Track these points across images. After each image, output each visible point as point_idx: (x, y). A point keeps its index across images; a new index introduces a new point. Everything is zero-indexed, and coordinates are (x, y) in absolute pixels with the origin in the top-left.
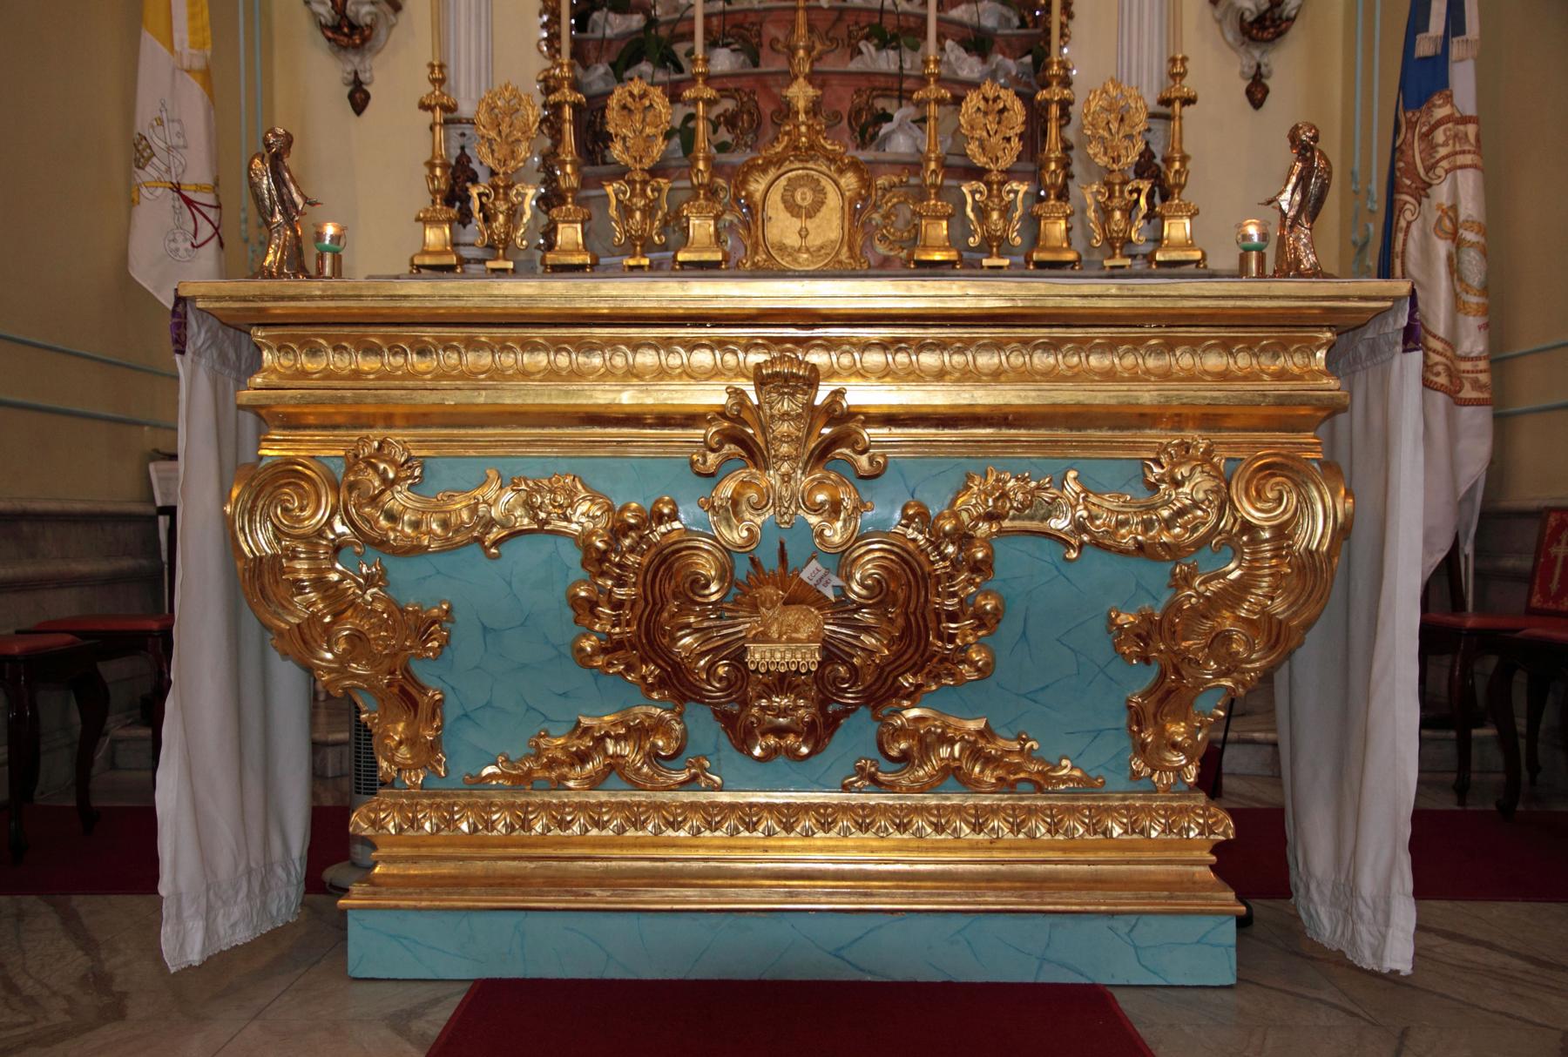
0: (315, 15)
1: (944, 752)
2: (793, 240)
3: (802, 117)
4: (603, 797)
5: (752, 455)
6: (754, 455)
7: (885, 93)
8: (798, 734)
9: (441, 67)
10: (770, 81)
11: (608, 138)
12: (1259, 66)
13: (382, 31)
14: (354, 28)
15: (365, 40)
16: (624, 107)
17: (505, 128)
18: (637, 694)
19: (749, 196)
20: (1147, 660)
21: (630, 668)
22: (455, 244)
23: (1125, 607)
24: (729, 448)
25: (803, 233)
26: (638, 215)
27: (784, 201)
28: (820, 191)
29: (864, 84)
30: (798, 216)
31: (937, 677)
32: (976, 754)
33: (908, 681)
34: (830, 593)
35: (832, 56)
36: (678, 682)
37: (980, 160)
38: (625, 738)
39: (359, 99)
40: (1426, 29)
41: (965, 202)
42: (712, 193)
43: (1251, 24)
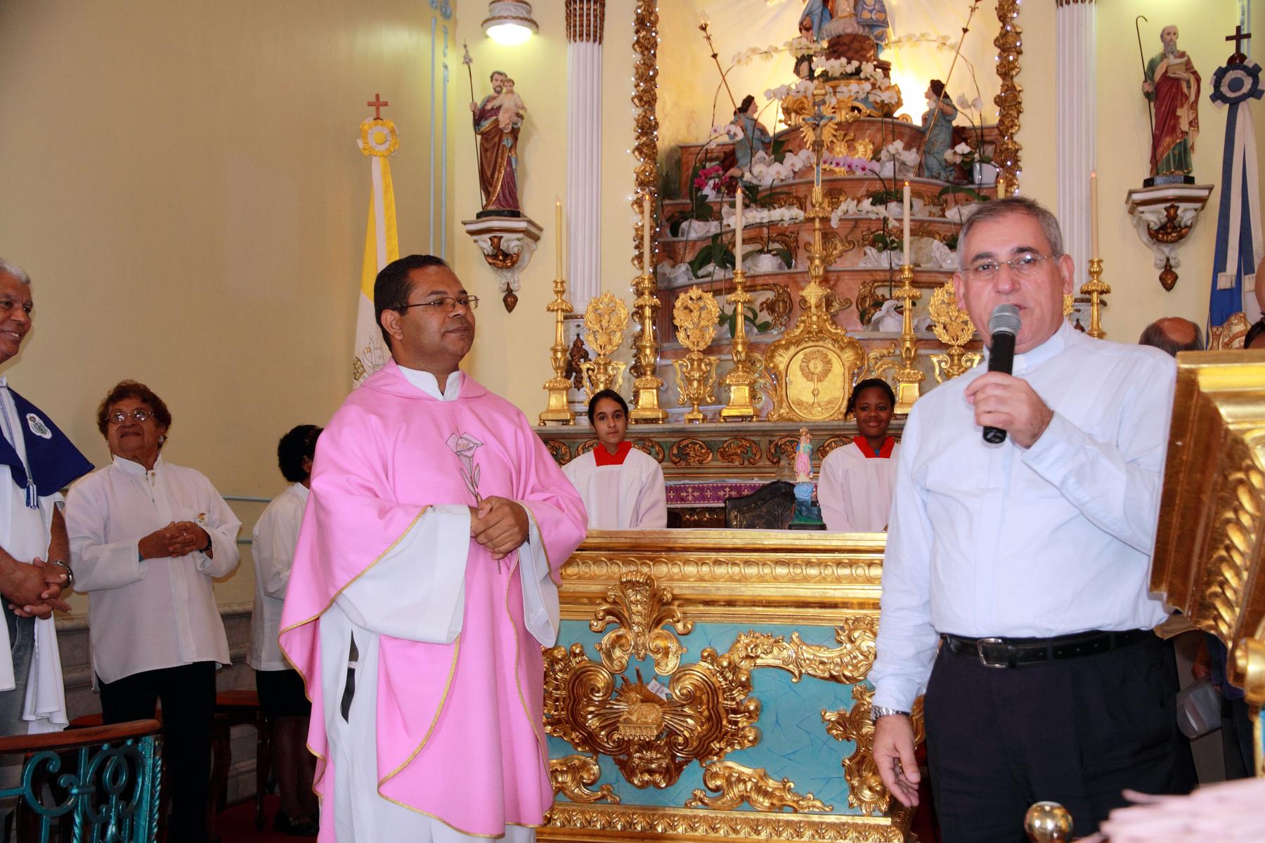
0: (482, 248)
1: (741, 787)
2: (808, 398)
3: (813, 310)
4: (737, 815)
5: (622, 622)
6: (623, 621)
7: (883, 283)
8: (660, 773)
9: (562, 283)
10: (799, 278)
11: (676, 328)
12: (1168, 260)
13: (526, 255)
14: (506, 255)
15: (513, 263)
16: (686, 308)
17: (605, 324)
18: (570, 747)
19: (776, 367)
20: (848, 739)
21: (565, 734)
22: (570, 402)
23: (831, 708)
24: (609, 618)
25: (815, 393)
26: (695, 384)
27: (802, 369)
28: (828, 362)
29: (868, 278)
30: (812, 380)
31: (732, 745)
32: (759, 790)
33: (716, 746)
34: (664, 698)
35: (850, 254)
36: (590, 741)
37: (945, 338)
38: (566, 772)
39: (510, 301)
40: (1224, 270)
41: (933, 368)
42: (749, 363)
43: (1157, 231)
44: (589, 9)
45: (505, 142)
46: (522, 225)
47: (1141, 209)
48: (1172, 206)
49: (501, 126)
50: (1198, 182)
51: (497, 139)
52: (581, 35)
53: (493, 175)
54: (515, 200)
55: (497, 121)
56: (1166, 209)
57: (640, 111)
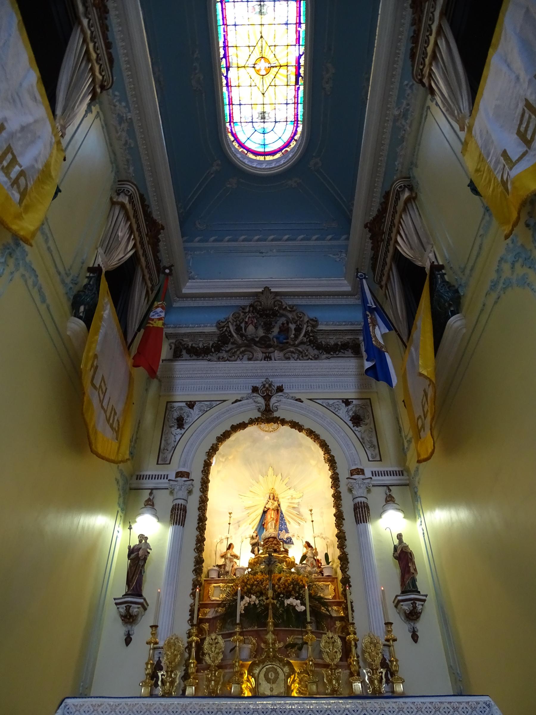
3: (271, 646)
14: (131, 616)
15: (133, 620)
25: (271, 690)
44: (180, 513)
45: (140, 563)
46: (142, 601)
47: (402, 603)
48: (414, 602)
49: (140, 555)
50: (421, 593)
51: (137, 562)
52: (176, 523)
53: (132, 578)
54: (141, 590)
55: (138, 554)
56: (412, 603)
57: (197, 554)
